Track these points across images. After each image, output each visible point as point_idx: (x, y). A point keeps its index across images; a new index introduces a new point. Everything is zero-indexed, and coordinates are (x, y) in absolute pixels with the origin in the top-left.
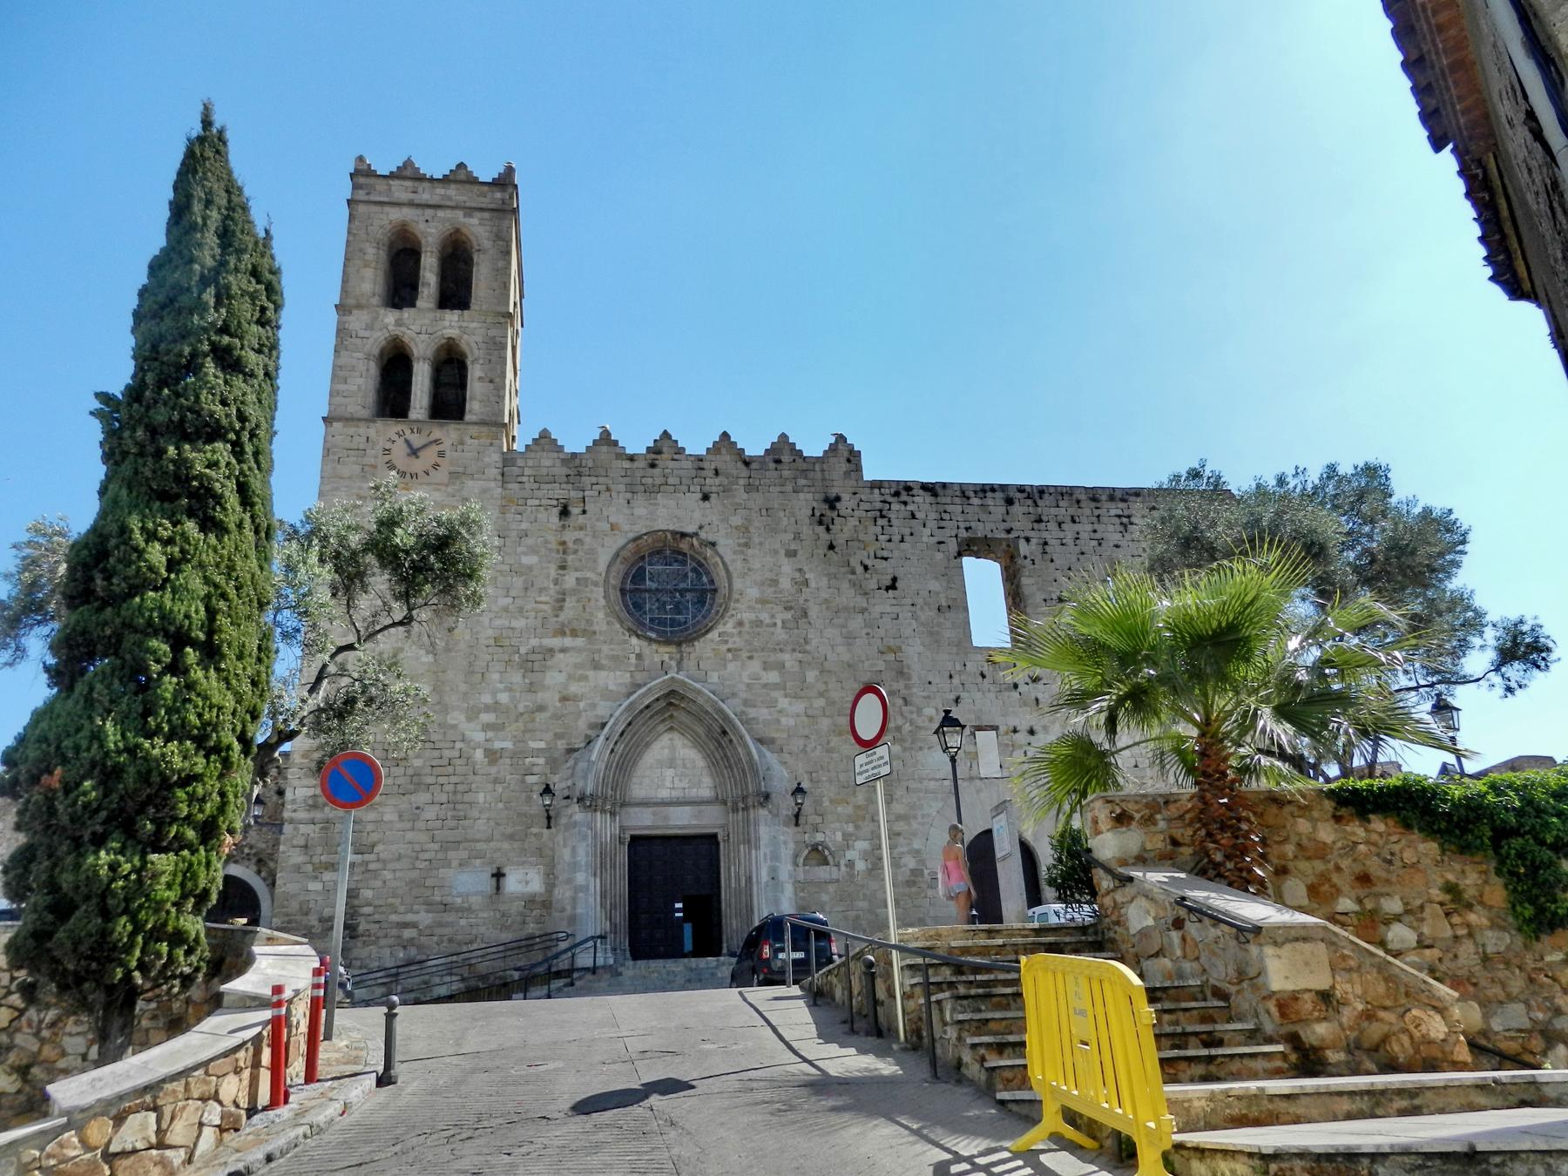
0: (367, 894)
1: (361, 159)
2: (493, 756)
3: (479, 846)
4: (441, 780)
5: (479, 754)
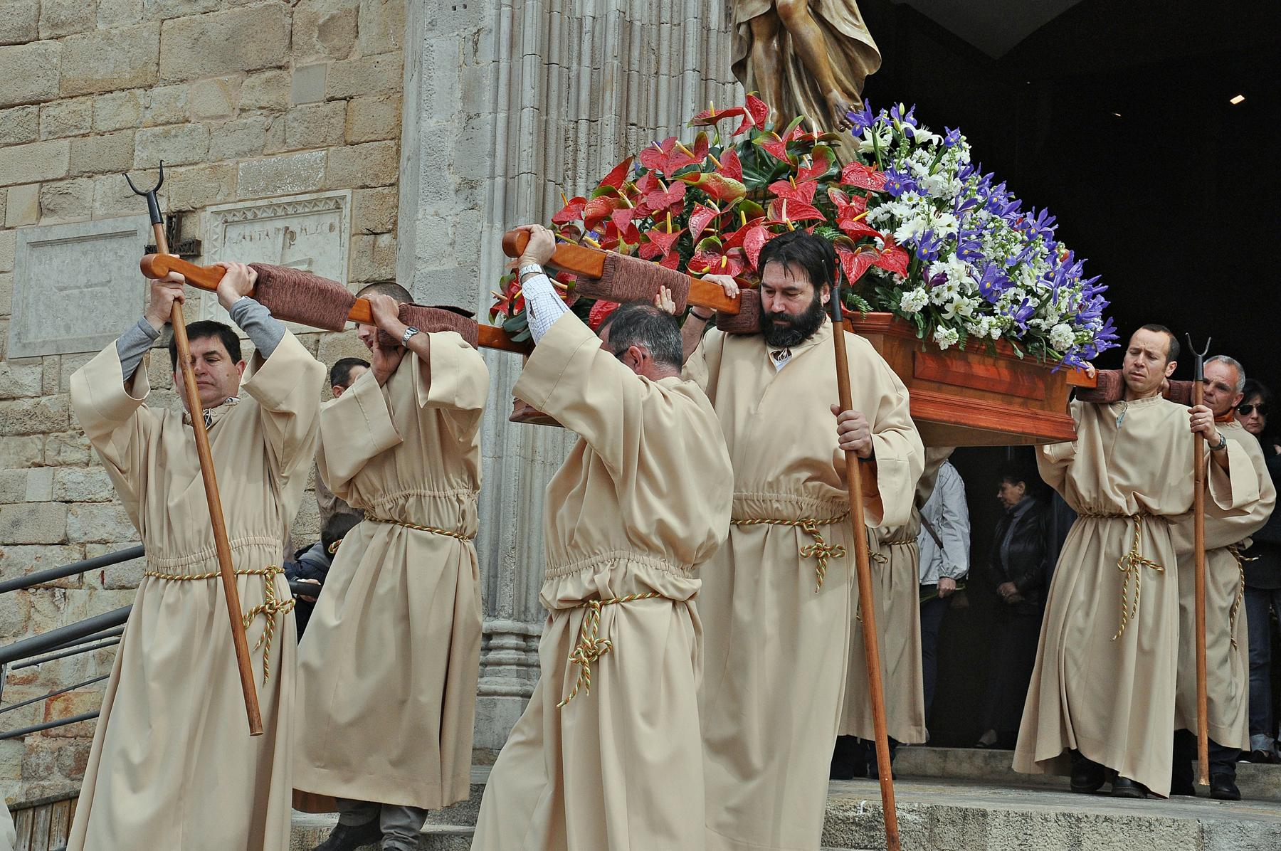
3: (110, 112)
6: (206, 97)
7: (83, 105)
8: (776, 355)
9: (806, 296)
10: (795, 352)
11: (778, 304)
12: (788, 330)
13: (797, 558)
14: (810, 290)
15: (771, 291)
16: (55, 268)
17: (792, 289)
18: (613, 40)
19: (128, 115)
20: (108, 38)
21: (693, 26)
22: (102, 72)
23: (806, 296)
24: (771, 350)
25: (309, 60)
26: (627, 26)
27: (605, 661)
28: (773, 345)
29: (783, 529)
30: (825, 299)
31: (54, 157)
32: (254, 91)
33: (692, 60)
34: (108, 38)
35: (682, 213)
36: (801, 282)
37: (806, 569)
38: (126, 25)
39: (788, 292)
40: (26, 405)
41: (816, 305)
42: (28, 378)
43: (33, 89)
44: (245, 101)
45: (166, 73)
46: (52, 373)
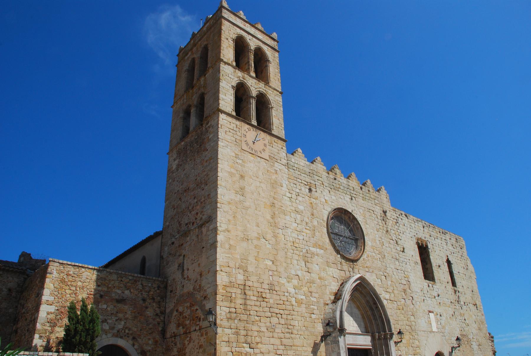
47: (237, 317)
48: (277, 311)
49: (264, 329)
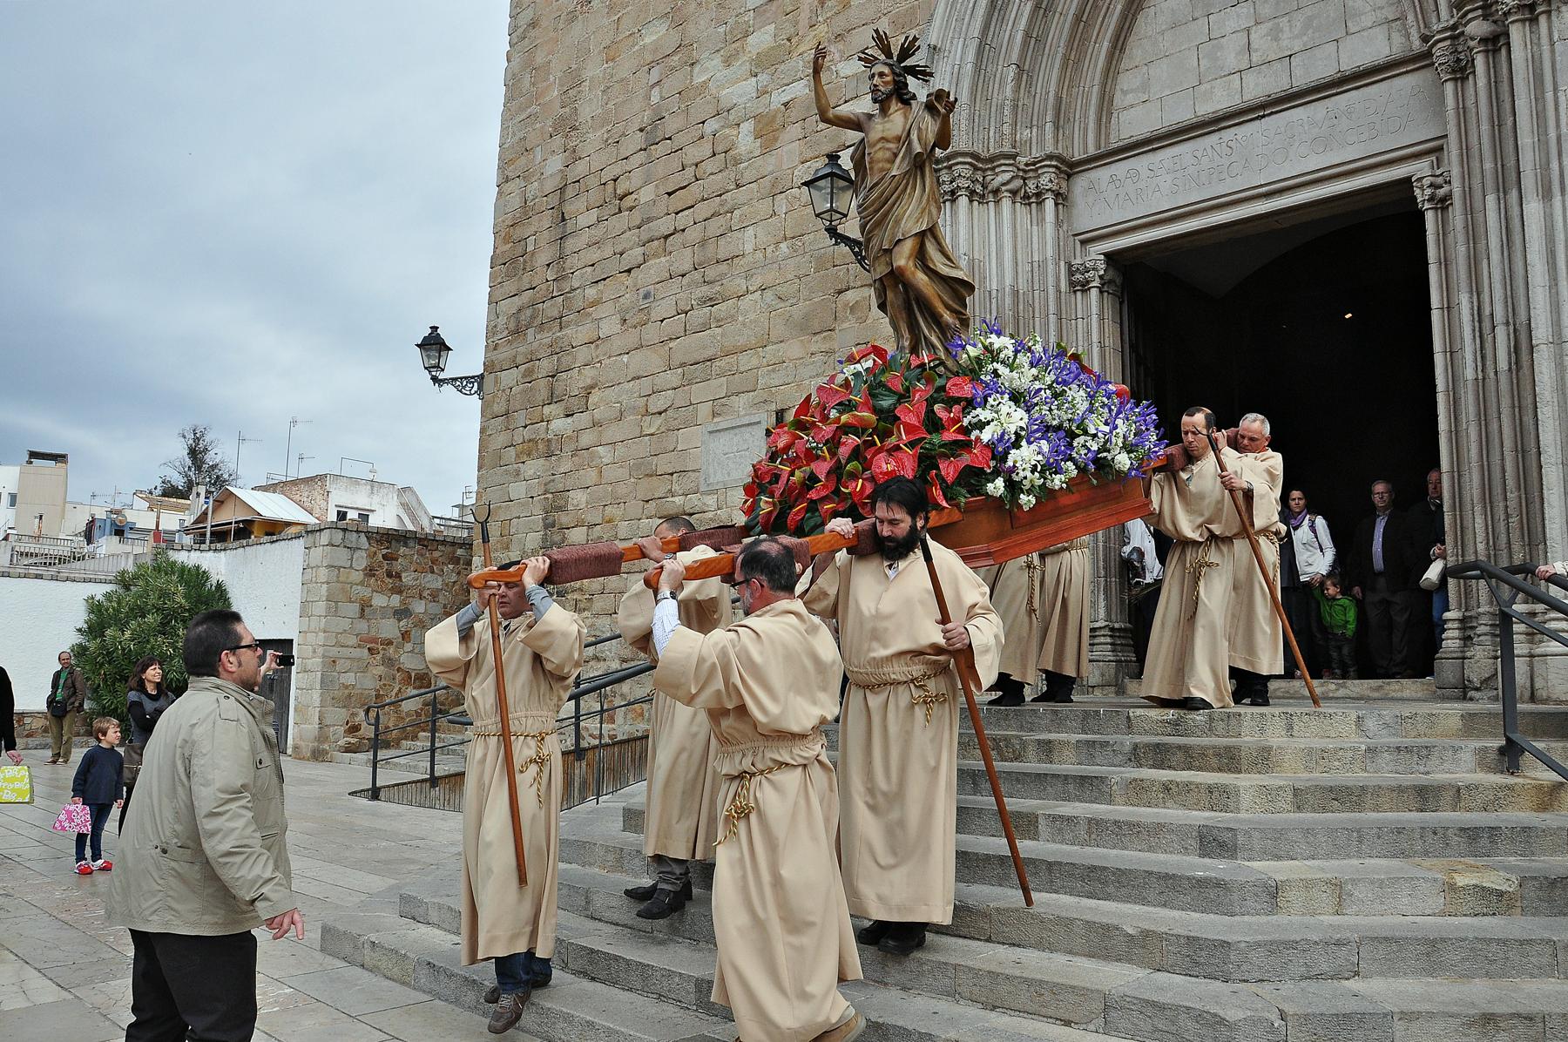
0: (578, 498)
1: (435, 328)
2: (768, 129)
3: (746, 361)
4: (684, 219)
5: (745, 139)
6: (793, 349)
7: (732, 359)
8: (890, 567)
9: (905, 523)
10: (902, 564)
11: (885, 531)
12: (896, 548)
13: (912, 706)
14: (908, 519)
15: (882, 522)
16: (722, 443)
17: (894, 520)
18: (1008, 301)
19: (755, 362)
20: (744, 324)
21: (1051, 290)
22: (742, 341)
23: (905, 523)
24: (886, 563)
25: (846, 325)
26: (1015, 293)
27: (753, 817)
28: (888, 559)
29: (901, 688)
30: (920, 524)
31: (718, 386)
32: (817, 344)
33: (1052, 309)
34: (744, 324)
35: (833, 443)
36: (900, 514)
37: (919, 712)
38: (752, 316)
39: (893, 522)
40: (710, 515)
41: (913, 528)
42: (711, 501)
43: (708, 353)
44: (813, 349)
45: (773, 338)
46: (722, 498)
47: (533, 317)
48: (664, 225)
49: (609, 327)
